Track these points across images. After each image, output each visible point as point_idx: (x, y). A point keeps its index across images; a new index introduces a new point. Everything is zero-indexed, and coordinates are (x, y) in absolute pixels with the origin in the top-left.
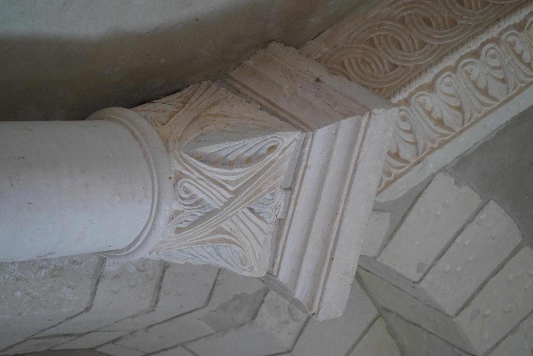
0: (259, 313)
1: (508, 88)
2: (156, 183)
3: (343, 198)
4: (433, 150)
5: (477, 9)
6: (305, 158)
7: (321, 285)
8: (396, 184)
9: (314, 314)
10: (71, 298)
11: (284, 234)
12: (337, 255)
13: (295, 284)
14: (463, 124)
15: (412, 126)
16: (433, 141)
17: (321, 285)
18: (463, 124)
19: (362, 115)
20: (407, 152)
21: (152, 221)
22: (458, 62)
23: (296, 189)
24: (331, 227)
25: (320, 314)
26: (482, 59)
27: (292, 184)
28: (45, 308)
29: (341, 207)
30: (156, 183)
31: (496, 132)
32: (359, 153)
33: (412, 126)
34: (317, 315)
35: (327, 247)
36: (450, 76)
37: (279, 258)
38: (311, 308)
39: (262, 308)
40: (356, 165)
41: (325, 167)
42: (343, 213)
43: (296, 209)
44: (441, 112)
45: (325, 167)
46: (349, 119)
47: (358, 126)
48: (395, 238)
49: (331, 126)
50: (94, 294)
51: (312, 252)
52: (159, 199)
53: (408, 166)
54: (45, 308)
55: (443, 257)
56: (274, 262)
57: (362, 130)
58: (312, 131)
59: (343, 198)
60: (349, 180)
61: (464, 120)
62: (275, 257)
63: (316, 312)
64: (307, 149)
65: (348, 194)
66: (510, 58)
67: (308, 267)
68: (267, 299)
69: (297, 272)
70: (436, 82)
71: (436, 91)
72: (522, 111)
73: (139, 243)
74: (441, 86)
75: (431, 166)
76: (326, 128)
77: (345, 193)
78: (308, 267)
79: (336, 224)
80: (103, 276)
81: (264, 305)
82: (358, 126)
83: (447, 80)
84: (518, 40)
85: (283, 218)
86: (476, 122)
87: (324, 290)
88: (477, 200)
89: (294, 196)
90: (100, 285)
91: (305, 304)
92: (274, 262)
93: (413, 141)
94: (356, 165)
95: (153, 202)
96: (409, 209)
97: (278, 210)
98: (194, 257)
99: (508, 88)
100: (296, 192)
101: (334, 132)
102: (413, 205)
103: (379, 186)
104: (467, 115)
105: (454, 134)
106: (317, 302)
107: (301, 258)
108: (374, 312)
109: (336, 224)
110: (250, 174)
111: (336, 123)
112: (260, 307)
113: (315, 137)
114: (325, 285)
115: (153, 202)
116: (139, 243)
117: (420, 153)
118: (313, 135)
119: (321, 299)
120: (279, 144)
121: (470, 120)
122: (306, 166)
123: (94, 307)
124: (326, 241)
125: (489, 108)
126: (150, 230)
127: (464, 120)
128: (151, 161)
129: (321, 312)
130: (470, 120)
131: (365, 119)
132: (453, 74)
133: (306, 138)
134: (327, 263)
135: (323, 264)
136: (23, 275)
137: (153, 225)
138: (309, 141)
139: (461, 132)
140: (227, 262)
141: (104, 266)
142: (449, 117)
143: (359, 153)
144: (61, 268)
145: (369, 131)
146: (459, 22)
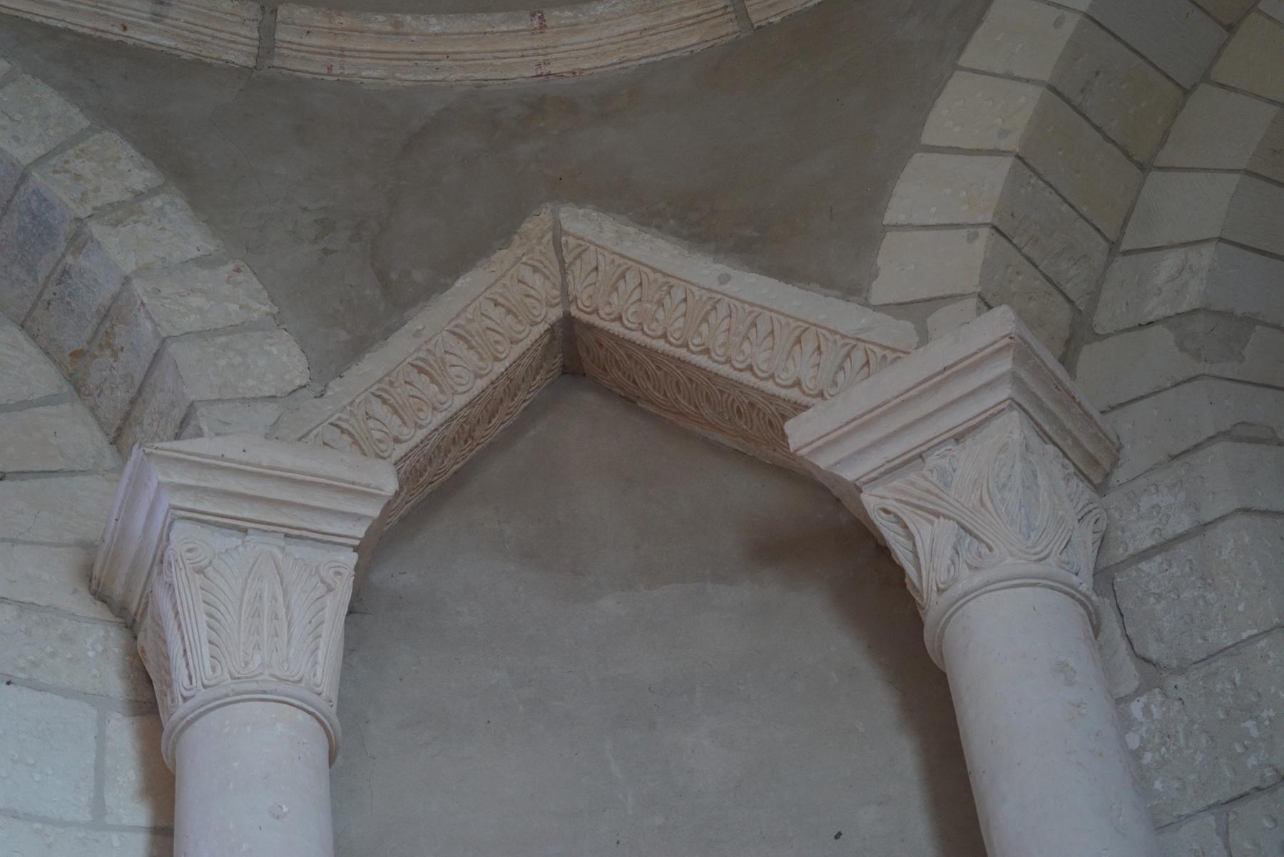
0: (1189, 310)
1: (757, 317)
2: (949, 613)
3: (885, 408)
4: (843, 336)
5: (729, 395)
6: (882, 470)
7: (979, 356)
8: (889, 344)
9: (1011, 338)
10: (1232, 541)
11: (965, 426)
12: (940, 368)
13: (1004, 375)
14: (807, 328)
15: (836, 373)
16: (835, 342)
17: (979, 356)
18: (807, 328)
19: (802, 457)
20: (858, 357)
21: (983, 590)
22: (765, 379)
23: (915, 452)
24: (920, 395)
25: (1007, 333)
26: (749, 361)
27: (916, 459)
28: (1249, 563)
29: (894, 402)
30: (949, 613)
31: (807, 287)
32: (836, 430)
33: (836, 373)
34: (1010, 334)
35: (941, 382)
36: (778, 376)
37: (991, 412)
38: (1008, 345)
39: (1183, 311)
40: (847, 423)
41: (875, 445)
42: (898, 396)
43: (933, 436)
44: (810, 357)
45: (875, 445)
46: (818, 464)
47: (819, 450)
48: (949, 292)
49: (836, 472)
50: (1222, 518)
51: (957, 389)
52: (957, 601)
53: (869, 346)
54: (1249, 563)
55: (955, 222)
56: (999, 413)
57: (814, 445)
58: (855, 485)
59: (885, 408)
60: (866, 417)
61: (805, 331)
62: (993, 415)
63: (1007, 338)
64: (874, 475)
65: (878, 407)
66: (734, 338)
67: (975, 381)
68: (1172, 313)
69: (988, 385)
70: (790, 384)
71: (797, 378)
72: (777, 281)
73: (1017, 582)
74: (786, 377)
75: (864, 320)
76: (842, 475)
77: (879, 410)
78: (975, 381)
79: (913, 393)
80: (1199, 523)
81: (1179, 311)
82: (819, 450)
83: (783, 376)
84: (717, 345)
85: (952, 441)
86: (797, 319)
87: (981, 350)
88: (891, 237)
89: (923, 448)
90: (1209, 519)
91: (1011, 352)
92: (999, 413)
93: (848, 359)
94: (847, 423)
95: (957, 610)
96: (918, 302)
97: (944, 453)
98: (1022, 504)
99: (757, 317)
100: (918, 451)
101: (838, 465)
102: (912, 302)
103: (899, 357)
104: (797, 333)
105: (819, 329)
106: (997, 346)
107: (973, 393)
108: (1154, 176)
109: (913, 393)
110: (916, 514)
111: (830, 470)
112: (1183, 313)
113: (856, 477)
114: (976, 353)
115: (957, 610)
116: (1017, 582)
117: (851, 346)
118: (857, 480)
119: (992, 344)
120: (878, 509)
121: (800, 327)
122: (889, 462)
123: (1236, 507)
124: (937, 387)
125: (780, 317)
126: (993, 583)
127: (805, 331)
128: (938, 630)
129: (1004, 334)
130: (800, 327)
131: (802, 452)
132: (776, 375)
133: (865, 483)
134: (955, 369)
135: (957, 372)
136: (1220, 617)
137: (986, 586)
138: (864, 479)
139: (814, 325)
140: (1013, 466)
141: (1186, 531)
142: (809, 346)
143: (836, 430)
144: (1202, 579)
145: (810, 440)
146: (747, 401)
